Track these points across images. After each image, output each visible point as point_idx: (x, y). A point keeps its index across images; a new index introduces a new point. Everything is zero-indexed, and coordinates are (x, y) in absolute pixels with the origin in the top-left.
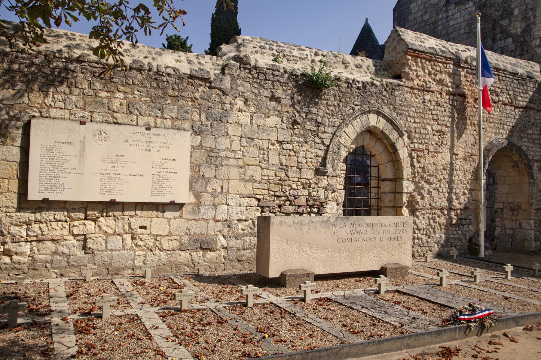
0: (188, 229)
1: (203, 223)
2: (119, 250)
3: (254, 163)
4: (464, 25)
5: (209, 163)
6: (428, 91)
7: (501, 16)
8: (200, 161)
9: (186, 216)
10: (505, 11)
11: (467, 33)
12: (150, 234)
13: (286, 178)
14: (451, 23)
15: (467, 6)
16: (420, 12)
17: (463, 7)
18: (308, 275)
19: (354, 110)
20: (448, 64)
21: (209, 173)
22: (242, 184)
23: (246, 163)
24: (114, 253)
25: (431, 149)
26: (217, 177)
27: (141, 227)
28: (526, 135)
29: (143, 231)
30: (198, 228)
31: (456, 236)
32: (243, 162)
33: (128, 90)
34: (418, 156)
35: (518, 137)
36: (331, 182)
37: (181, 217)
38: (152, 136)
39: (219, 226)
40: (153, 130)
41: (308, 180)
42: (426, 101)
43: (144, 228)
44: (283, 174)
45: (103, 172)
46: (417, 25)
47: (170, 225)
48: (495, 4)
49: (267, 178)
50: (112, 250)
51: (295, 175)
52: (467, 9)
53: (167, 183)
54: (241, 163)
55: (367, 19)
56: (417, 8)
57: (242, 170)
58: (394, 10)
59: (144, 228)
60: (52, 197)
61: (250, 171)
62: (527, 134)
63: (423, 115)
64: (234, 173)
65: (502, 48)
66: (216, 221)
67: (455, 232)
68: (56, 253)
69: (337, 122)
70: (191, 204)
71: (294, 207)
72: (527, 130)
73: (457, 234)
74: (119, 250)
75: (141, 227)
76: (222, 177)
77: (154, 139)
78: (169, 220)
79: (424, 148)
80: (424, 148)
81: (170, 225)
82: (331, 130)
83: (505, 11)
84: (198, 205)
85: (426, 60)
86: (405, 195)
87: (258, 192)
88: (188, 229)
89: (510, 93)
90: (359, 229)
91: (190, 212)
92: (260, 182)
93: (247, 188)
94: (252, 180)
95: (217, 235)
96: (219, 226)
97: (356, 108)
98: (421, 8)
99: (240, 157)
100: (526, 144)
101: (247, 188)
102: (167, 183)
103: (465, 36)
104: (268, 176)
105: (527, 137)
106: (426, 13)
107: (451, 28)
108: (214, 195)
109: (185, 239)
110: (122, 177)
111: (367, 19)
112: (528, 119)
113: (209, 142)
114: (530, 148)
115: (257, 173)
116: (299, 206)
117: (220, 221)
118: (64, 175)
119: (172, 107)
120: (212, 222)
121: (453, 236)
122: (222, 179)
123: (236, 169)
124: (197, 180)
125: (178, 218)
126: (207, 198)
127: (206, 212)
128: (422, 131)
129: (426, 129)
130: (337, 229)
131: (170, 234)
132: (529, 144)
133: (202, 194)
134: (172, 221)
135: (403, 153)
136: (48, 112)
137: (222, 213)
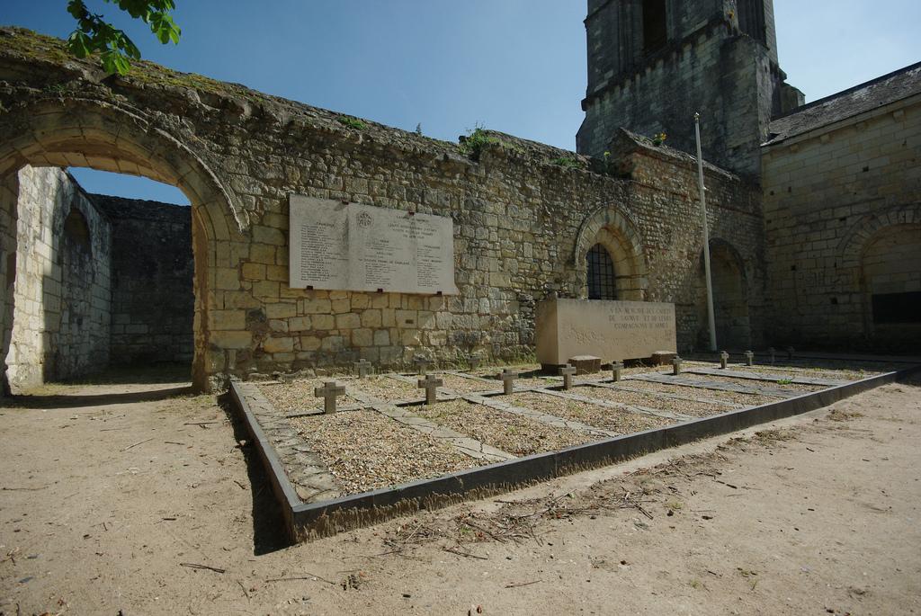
2: (386, 346)
15: (654, 125)
27: (408, 322)
29: (409, 325)
50: (379, 347)
53: (433, 273)
75: (408, 322)
118: (329, 261)
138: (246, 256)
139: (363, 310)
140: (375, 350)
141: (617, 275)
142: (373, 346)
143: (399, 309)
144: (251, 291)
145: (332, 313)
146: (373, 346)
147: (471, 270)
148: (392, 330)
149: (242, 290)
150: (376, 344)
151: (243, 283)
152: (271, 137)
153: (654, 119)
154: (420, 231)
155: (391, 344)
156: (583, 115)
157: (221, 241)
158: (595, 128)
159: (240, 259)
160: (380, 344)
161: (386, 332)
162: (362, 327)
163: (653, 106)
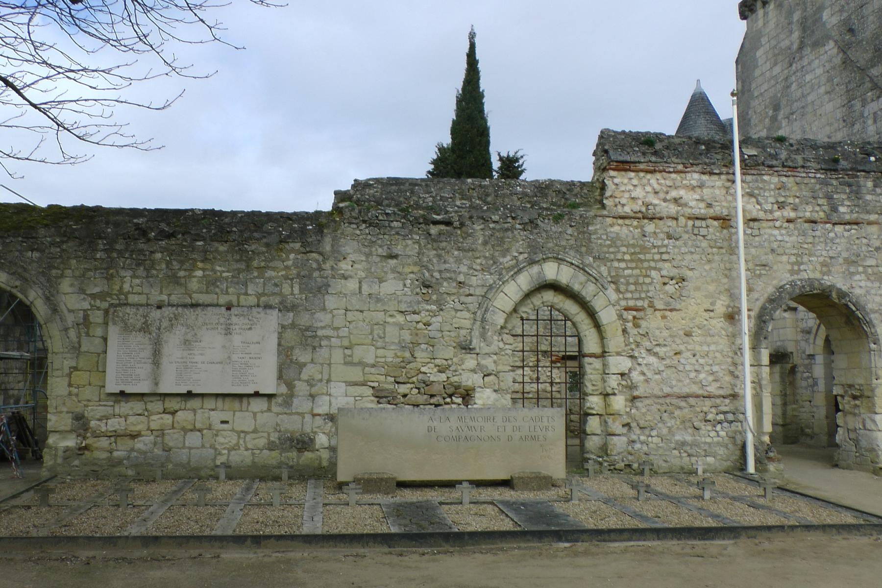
0: (277, 425)
1: (296, 417)
2: (198, 448)
3: (366, 341)
4: (823, 80)
5: (304, 345)
6: (651, 219)
7: (871, 60)
8: (293, 343)
9: (275, 409)
10: (876, 51)
11: (829, 92)
12: (233, 430)
13: (412, 359)
14: (808, 78)
15: (827, 48)
16: (768, 63)
17: (822, 50)
18: (387, 480)
19: (517, 260)
20: (688, 172)
21: (303, 356)
22: (350, 369)
23: (354, 342)
24: (192, 451)
25: (659, 305)
26: (315, 361)
27: (223, 422)
28: (861, 269)
29: (225, 426)
30: (292, 424)
31: (715, 439)
32: (350, 342)
33: (208, 266)
34: (634, 317)
35: (844, 273)
36: (483, 362)
37: (269, 410)
38: (233, 317)
39: (319, 421)
40: (234, 311)
41: (446, 360)
42: (647, 234)
43: (226, 422)
44: (407, 355)
45: (179, 360)
46: (766, 84)
47: (255, 420)
48: (862, 41)
49: (383, 360)
50: (190, 448)
51: (425, 354)
52: (826, 52)
53: (250, 371)
54: (346, 343)
55: (698, 81)
56: (764, 57)
57: (348, 352)
58: (737, 62)
59: (226, 422)
60: (129, 390)
61: (359, 353)
62: (864, 267)
63: (642, 256)
64: (338, 356)
65: (875, 113)
66: (314, 415)
67: (713, 434)
68: (132, 450)
69: (490, 279)
70: (282, 395)
71: (426, 396)
72: (863, 260)
73: (718, 436)
74: (198, 448)
75: (223, 422)
76: (321, 362)
77: (234, 320)
78: (255, 414)
79: (646, 306)
80: (646, 306)
81: (255, 420)
82: (480, 291)
83: (876, 51)
84: (290, 396)
85: (647, 172)
86: (614, 377)
87: (372, 378)
88: (277, 425)
89: (820, 203)
90: (471, 424)
91: (280, 405)
92: (373, 366)
93: (356, 374)
94: (362, 364)
95: (315, 433)
96: (319, 421)
97: (521, 257)
98: (770, 56)
99: (345, 335)
100: (863, 284)
101: (356, 374)
102: (250, 371)
103: (826, 97)
104: (603, 354)
105: (865, 272)
106: (776, 64)
107: (808, 86)
108: (310, 383)
109: (274, 437)
110: (200, 366)
111: (698, 81)
112: (864, 241)
113: (304, 320)
114: (873, 292)
115: (369, 355)
116: (432, 396)
117: (319, 415)
118: (139, 365)
119: (257, 280)
120: (308, 418)
121: (708, 440)
122: (322, 364)
123: (340, 351)
124: (288, 368)
125: (265, 411)
126: (301, 388)
127: (301, 404)
128: (641, 280)
129: (649, 276)
130: (435, 423)
131: (255, 431)
132: (869, 284)
133: (296, 382)
134: (258, 415)
135: (607, 316)
136: (126, 299)
137: (322, 407)
138: (74, 364)
139: (177, 411)
140: (185, 451)
141: (607, 372)
142: (184, 447)
143: (213, 410)
144: (77, 395)
145: (146, 414)
146: (184, 447)
147: (304, 365)
148: (205, 431)
149: (70, 394)
150: (187, 444)
151: (71, 389)
152: (250, 571)
153: (828, 37)
154: (237, 327)
155: (203, 446)
156: (326, 204)
157: (56, 354)
158: (757, 49)
159: (70, 368)
160: (191, 445)
161: (198, 433)
162: (173, 428)
163: (826, 15)
